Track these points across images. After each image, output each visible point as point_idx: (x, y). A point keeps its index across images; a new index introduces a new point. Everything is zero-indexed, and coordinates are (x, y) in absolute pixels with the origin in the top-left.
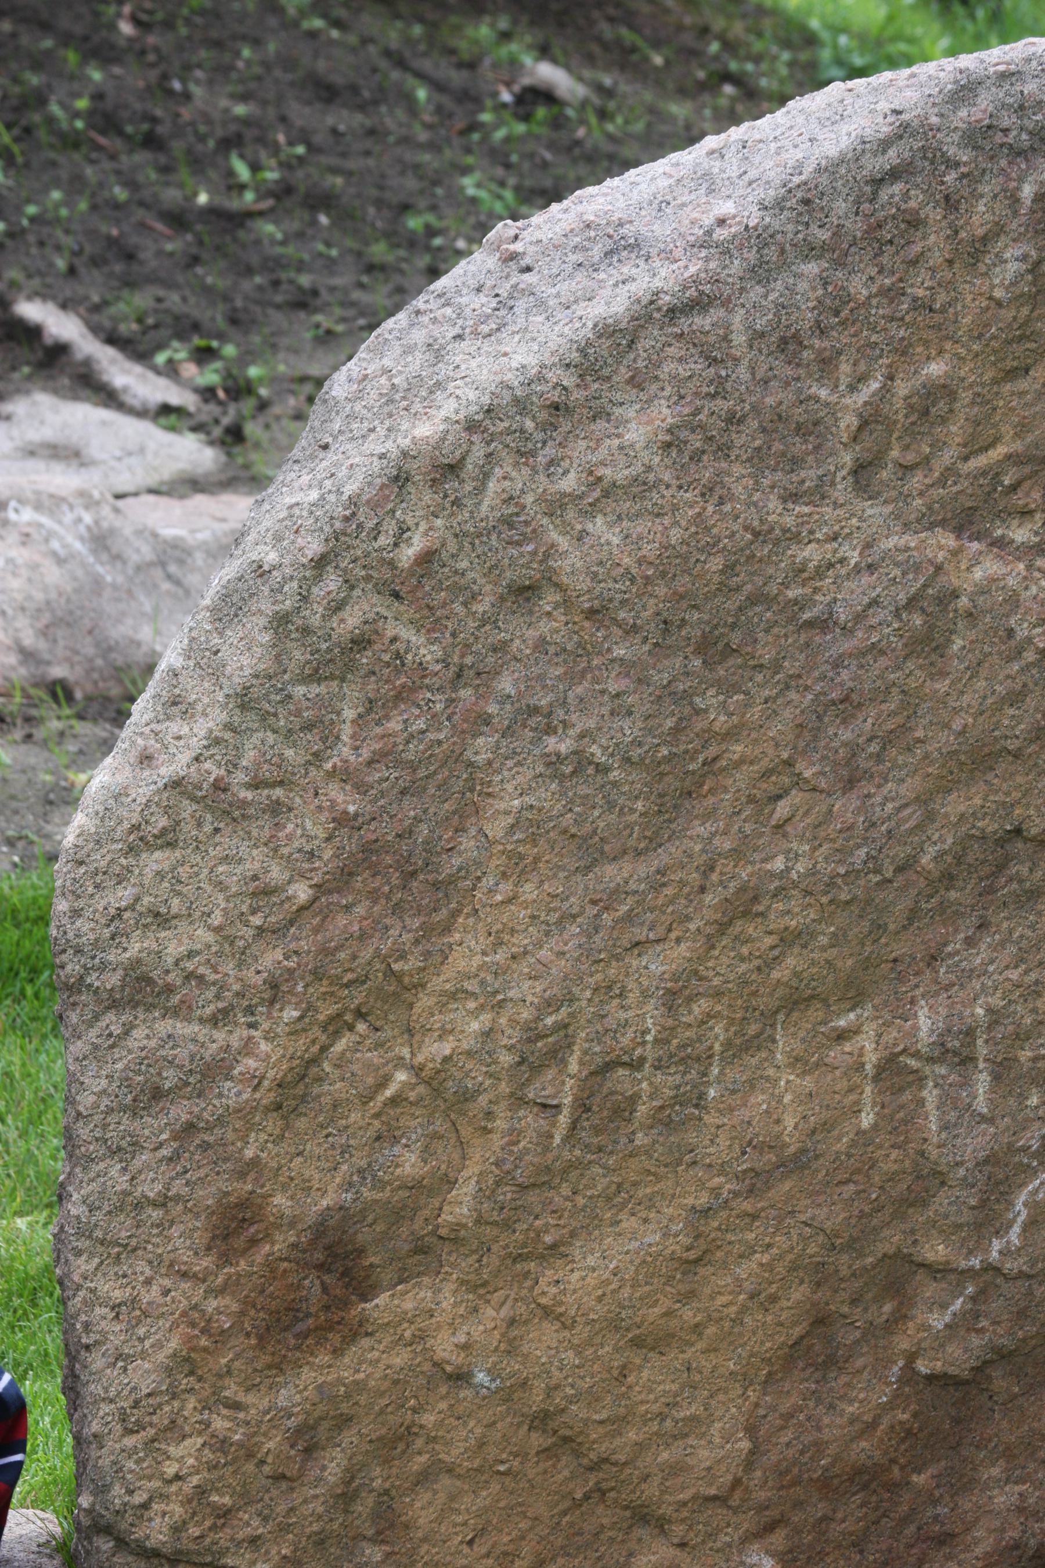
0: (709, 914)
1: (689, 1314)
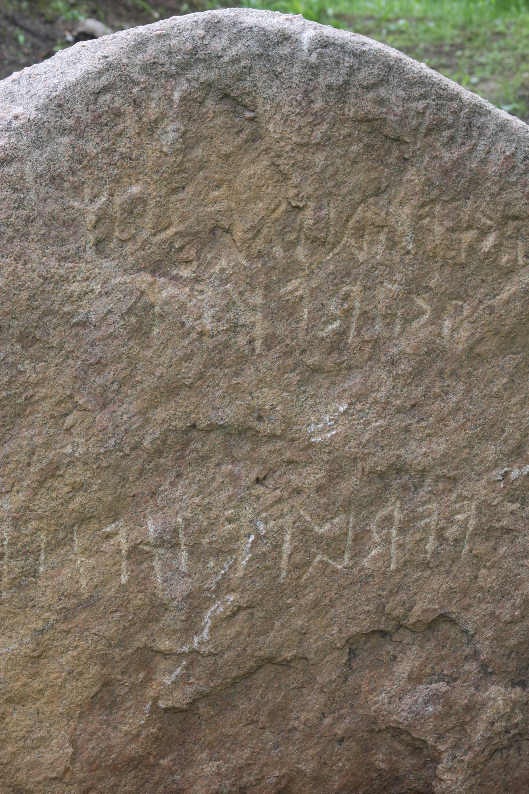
0: (33, 477)
1: (36, 685)
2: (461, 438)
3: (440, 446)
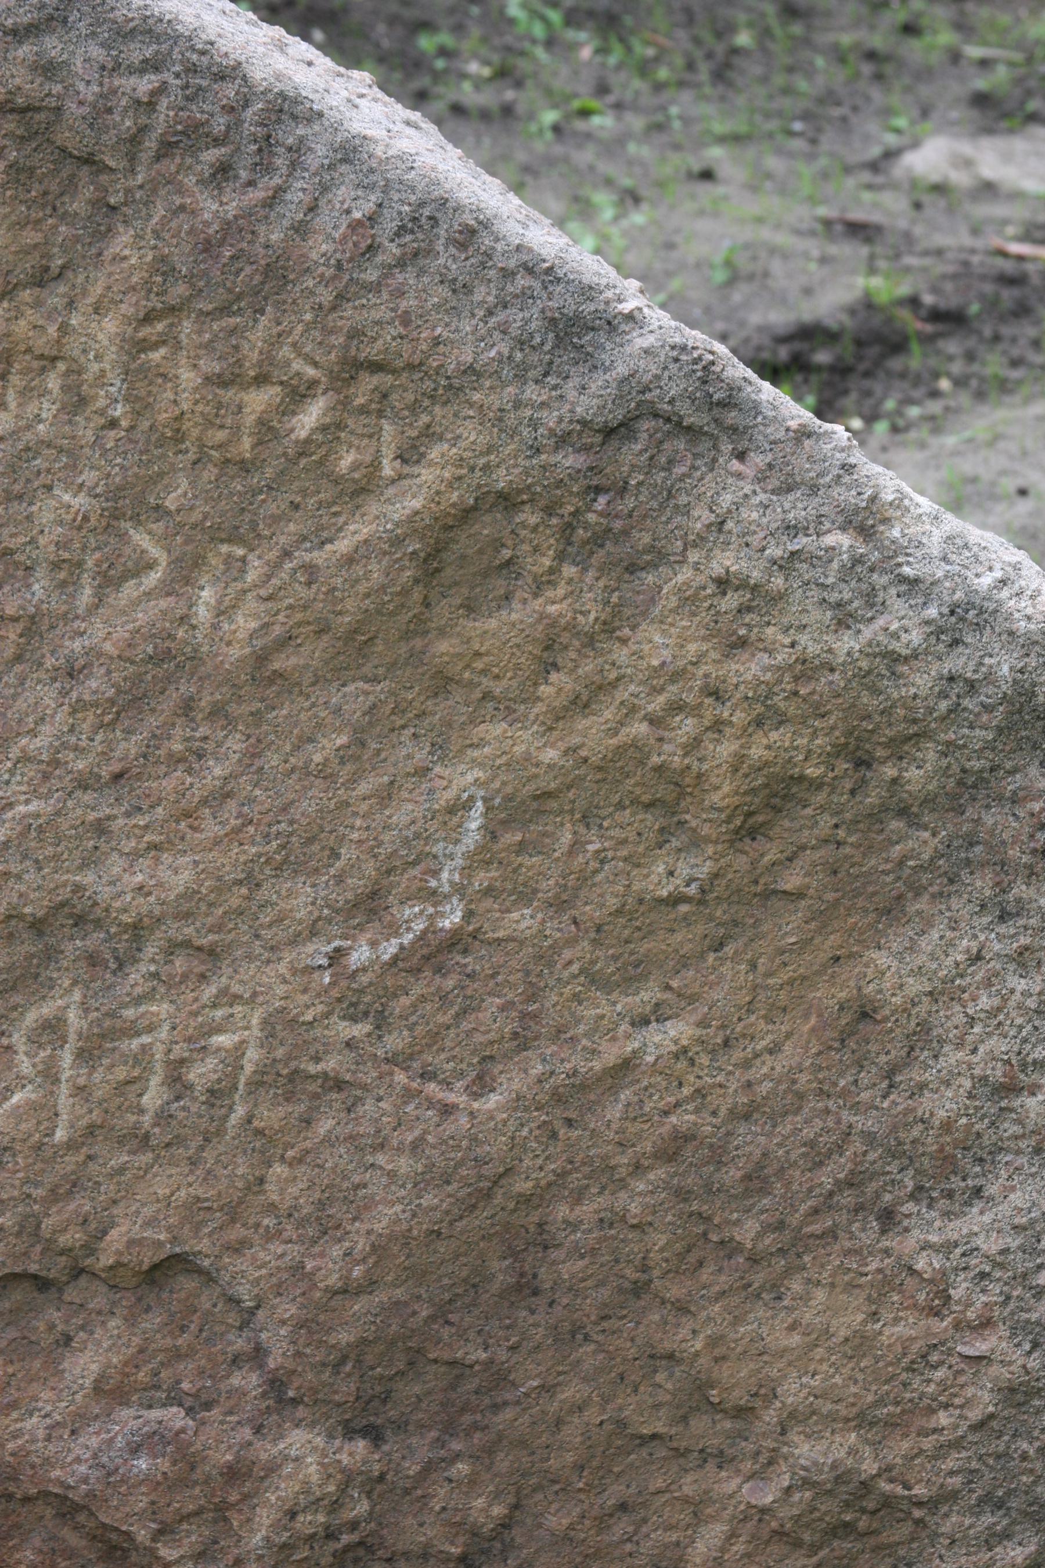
2: (228, 863)
3: (178, 875)
